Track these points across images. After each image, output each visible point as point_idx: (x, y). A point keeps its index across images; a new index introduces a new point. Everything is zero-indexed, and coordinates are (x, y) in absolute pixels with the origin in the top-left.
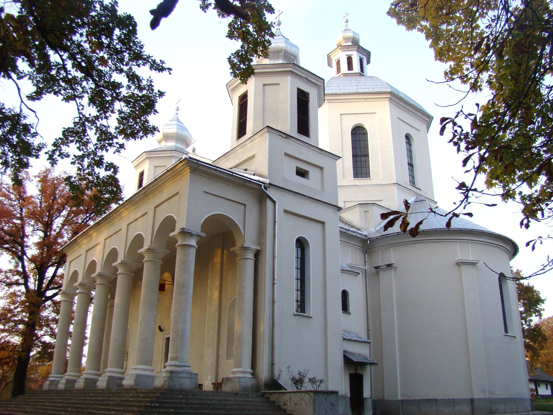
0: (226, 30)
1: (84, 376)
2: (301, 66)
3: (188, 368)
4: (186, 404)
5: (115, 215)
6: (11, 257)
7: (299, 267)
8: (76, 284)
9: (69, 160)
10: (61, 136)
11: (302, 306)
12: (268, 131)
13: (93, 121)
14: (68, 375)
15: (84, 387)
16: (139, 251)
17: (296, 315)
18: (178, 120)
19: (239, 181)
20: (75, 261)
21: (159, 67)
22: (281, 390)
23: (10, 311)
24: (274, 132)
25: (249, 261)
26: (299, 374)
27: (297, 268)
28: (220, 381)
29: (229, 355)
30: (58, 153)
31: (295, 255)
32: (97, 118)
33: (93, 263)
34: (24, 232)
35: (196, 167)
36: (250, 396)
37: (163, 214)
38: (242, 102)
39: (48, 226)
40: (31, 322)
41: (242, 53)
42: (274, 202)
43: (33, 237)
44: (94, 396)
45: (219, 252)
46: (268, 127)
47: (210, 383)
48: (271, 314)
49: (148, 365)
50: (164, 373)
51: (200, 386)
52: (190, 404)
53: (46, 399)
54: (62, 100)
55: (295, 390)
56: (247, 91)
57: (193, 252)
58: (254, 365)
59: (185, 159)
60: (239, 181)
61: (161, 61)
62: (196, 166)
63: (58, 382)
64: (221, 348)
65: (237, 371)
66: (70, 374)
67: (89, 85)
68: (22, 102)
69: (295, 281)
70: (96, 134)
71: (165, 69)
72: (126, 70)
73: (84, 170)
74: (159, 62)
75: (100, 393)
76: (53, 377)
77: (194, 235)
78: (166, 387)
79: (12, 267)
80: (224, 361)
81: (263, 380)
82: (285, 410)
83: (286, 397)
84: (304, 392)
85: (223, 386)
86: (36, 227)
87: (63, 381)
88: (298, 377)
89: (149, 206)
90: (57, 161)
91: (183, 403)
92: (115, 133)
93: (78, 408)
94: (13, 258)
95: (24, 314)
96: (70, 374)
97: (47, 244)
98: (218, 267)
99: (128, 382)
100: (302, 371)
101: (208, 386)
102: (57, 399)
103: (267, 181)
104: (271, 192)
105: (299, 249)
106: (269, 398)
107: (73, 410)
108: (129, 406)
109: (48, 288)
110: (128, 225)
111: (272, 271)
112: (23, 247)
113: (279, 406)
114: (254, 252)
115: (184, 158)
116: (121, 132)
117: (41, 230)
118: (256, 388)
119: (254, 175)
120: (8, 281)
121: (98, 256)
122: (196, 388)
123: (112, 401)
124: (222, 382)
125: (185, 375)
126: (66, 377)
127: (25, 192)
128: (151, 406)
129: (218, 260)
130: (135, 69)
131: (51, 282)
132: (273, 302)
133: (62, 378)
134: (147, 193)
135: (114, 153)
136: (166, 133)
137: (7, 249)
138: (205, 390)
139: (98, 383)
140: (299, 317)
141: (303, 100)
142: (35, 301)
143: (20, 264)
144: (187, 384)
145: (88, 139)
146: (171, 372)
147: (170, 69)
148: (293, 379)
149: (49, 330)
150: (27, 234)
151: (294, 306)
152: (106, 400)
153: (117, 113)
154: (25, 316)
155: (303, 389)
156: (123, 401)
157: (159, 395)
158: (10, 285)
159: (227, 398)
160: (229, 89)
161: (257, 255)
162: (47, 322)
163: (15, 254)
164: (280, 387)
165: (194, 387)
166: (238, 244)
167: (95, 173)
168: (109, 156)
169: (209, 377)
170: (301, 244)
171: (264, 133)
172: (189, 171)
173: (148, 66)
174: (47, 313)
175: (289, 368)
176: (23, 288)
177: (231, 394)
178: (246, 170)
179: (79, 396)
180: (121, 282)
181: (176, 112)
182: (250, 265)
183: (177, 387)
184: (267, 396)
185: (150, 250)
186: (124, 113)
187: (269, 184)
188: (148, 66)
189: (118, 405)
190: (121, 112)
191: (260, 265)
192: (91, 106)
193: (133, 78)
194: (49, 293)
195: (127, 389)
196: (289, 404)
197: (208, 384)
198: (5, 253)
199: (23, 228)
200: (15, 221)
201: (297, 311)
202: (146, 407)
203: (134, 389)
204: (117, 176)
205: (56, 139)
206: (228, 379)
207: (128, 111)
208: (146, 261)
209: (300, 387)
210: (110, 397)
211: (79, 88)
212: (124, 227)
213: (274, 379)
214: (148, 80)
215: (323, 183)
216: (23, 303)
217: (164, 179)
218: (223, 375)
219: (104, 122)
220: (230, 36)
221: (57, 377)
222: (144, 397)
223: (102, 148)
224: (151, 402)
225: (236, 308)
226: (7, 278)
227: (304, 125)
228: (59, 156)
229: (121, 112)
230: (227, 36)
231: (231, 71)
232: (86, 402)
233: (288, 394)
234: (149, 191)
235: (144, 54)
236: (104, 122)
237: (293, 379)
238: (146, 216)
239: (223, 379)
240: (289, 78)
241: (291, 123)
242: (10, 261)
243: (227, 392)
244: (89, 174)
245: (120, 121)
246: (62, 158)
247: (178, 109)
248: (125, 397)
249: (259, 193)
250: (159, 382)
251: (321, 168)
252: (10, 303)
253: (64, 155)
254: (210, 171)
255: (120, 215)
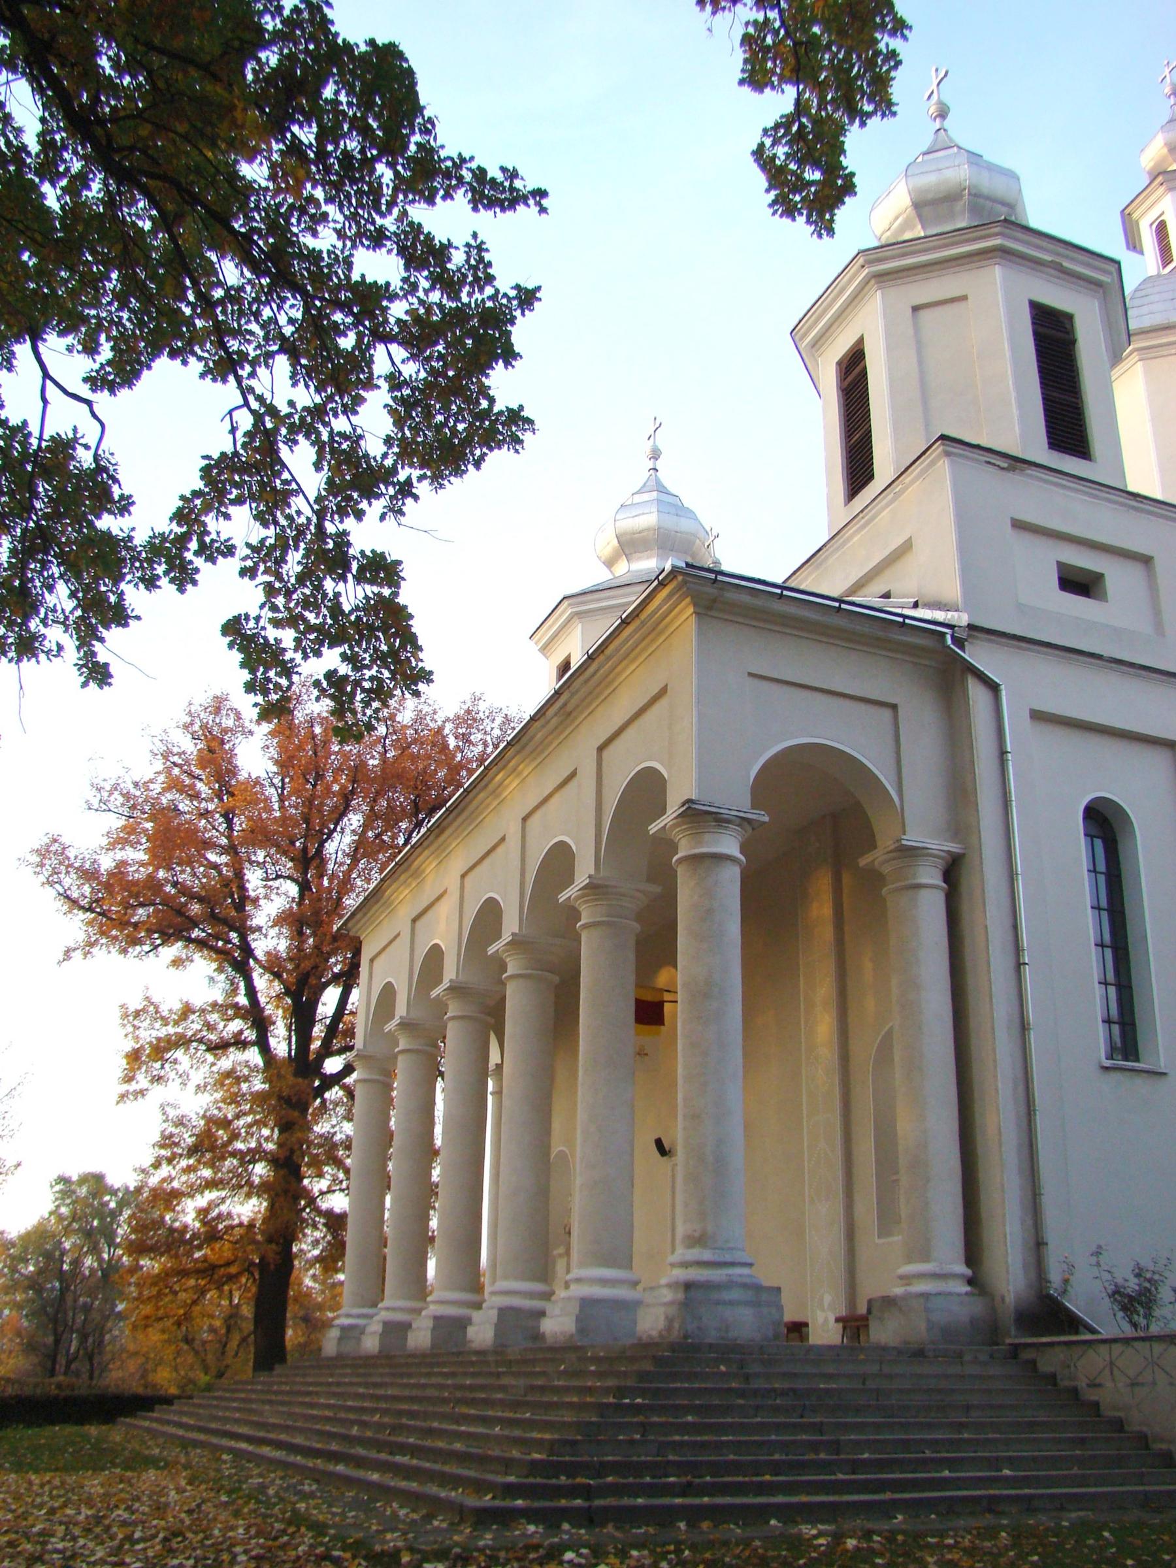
0: (737, 58)
1: (433, 1309)
2: (1034, 223)
3: (745, 1271)
4: (742, 1394)
5: (482, 795)
6: (214, 965)
7: (1104, 903)
8: (391, 1026)
9: (229, 566)
10: (199, 485)
11: (1126, 1038)
12: (947, 454)
13: (308, 423)
14: (387, 1309)
15: (433, 1346)
16: (563, 897)
17: (1107, 1068)
18: (661, 489)
19: (865, 628)
20: (383, 956)
21: (496, 193)
22: (1077, 1333)
23: (225, 1123)
24: (968, 452)
25: (924, 894)
26: (1138, 1275)
27: (1097, 908)
28: (862, 1309)
29: (887, 1220)
30: (194, 545)
31: (1085, 864)
32: (319, 412)
33: (436, 953)
34: (242, 888)
35: (708, 593)
36: (967, 1358)
37: (622, 771)
38: (850, 379)
39: (308, 862)
40: (282, 1155)
41: (802, 126)
42: (994, 688)
43: (272, 897)
44: (453, 1375)
45: (822, 884)
46: (943, 437)
47: (832, 1319)
48: (1020, 1074)
49: (620, 1267)
50: (665, 1291)
51: (798, 1328)
52: (756, 1392)
53: (321, 1384)
54: (203, 376)
55: (1128, 1331)
56: (861, 340)
57: (730, 880)
58: (973, 1251)
59: (675, 571)
60: (865, 628)
61: (503, 169)
62: (711, 590)
63: (362, 1330)
64: (857, 1197)
65: (918, 1272)
66: (393, 1306)
67: (289, 313)
68: (46, 375)
69: (1094, 952)
70: (318, 467)
71: (524, 199)
72: (393, 228)
73: (288, 594)
74: (500, 177)
75: (472, 1363)
76: (348, 1316)
77: (728, 821)
78: (675, 1335)
79: (217, 994)
80: (870, 1242)
81: (1010, 1299)
82: (1096, 1405)
83: (1097, 1359)
84: (1160, 1338)
85: (874, 1326)
86: (271, 870)
87: (375, 1327)
88: (1133, 1285)
89: (578, 753)
90: (197, 570)
91: (730, 1390)
92: (385, 456)
93: (400, 1413)
94: (220, 970)
95: (266, 1132)
96: (393, 1306)
97: (310, 918)
98: (827, 933)
99: (558, 1323)
100: (1146, 1262)
101: (825, 1329)
102: (352, 1384)
103: (962, 619)
104: (977, 655)
105: (1098, 843)
106: (1034, 1362)
107: (386, 1420)
108: (550, 1406)
109: (327, 1051)
110: (524, 819)
111: (1008, 922)
112: (243, 933)
113: (1075, 1391)
114: (941, 864)
115: (668, 567)
116: (407, 450)
117: (289, 877)
118: (988, 1331)
119: (916, 605)
120: (213, 1037)
121: (445, 930)
122: (776, 1336)
123: (503, 1388)
124: (869, 1311)
125: (735, 1294)
126: (384, 1315)
127: (233, 771)
128: (619, 1407)
129: (821, 909)
130: (419, 213)
131: (332, 1030)
132: (1024, 1027)
133: (370, 1317)
134: (569, 707)
135: (383, 517)
136: (625, 534)
137: (201, 944)
138: (819, 1342)
139: (471, 1331)
140: (1116, 1076)
141: (1053, 340)
142: (295, 1090)
143: (242, 984)
144: (744, 1323)
145: (286, 482)
146: (688, 1286)
147: (540, 194)
148: (1117, 1293)
149: (341, 1175)
150: (252, 894)
151: (1098, 1039)
152: (483, 1388)
153: (385, 386)
154: (267, 1139)
155: (1154, 1329)
156: (532, 1388)
157: (648, 1366)
158: (220, 1047)
159: (886, 1369)
160: (802, 346)
161: (953, 872)
162: (331, 1152)
163: (223, 955)
164: (1072, 1323)
165: (770, 1334)
166: (885, 842)
167: (325, 595)
168: (368, 533)
169: (827, 1299)
170: (1104, 823)
171: (933, 463)
172: (691, 610)
173: (461, 197)
174: (333, 1125)
175: (1097, 1253)
176: (253, 1056)
177: (900, 1352)
178: (887, 596)
179: (410, 1375)
180: (518, 1003)
181: (650, 464)
182: (930, 909)
183: (712, 1337)
184: (1027, 1355)
185: (594, 888)
186: (406, 383)
187: (971, 627)
188: (461, 197)
189: (516, 1405)
190: (395, 381)
191: (965, 907)
192: (302, 384)
193: (422, 252)
194: (333, 1065)
195: (551, 1349)
196: (1109, 1384)
197: (826, 1320)
198: (197, 956)
199: (239, 876)
200: (212, 857)
201: (1110, 1057)
202: (602, 1408)
203: (577, 1348)
204: (401, 600)
205: (183, 498)
206: (889, 1302)
207: (423, 375)
208: (585, 926)
209: (1142, 1322)
210: (498, 1375)
211: (254, 327)
212: (513, 829)
213: (1050, 1297)
214: (468, 245)
215: (1157, 611)
216: (259, 1098)
217: (617, 650)
218: (872, 1286)
219: (340, 424)
220: (756, 78)
221: (359, 1316)
222: (600, 1375)
223: (342, 513)
224: (620, 1392)
225: (897, 1058)
226: (210, 1027)
227: (1067, 421)
228: (197, 553)
229: (395, 381)
230: (742, 82)
231: (772, 195)
232: (429, 1392)
233: (1103, 1349)
234: (573, 702)
235: (443, 154)
236: (340, 424)
237: (1117, 1293)
238: (573, 784)
239: (870, 1302)
240: (996, 274)
241: (1013, 349)
242: (212, 979)
243: (884, 1349)
244: (306, 604)
245: (401, 412)
246: (212, 559)
247: (655, 455)
248: (544, 1373)
249: (940, 661)
250: (651, 1322)
251: (1146, 561)
252: (224, 1101)
253: (218, 550)
254: (758, 602)
255: (495, 793)
